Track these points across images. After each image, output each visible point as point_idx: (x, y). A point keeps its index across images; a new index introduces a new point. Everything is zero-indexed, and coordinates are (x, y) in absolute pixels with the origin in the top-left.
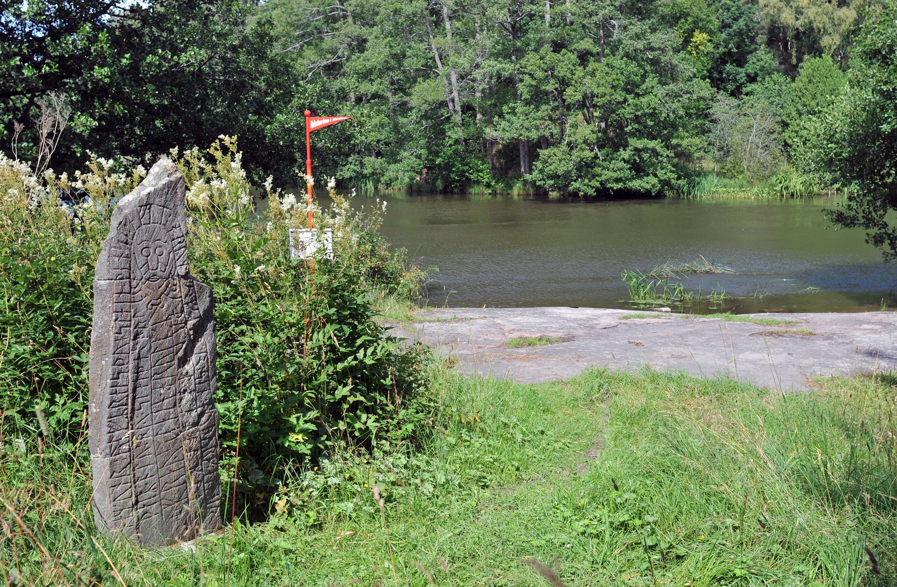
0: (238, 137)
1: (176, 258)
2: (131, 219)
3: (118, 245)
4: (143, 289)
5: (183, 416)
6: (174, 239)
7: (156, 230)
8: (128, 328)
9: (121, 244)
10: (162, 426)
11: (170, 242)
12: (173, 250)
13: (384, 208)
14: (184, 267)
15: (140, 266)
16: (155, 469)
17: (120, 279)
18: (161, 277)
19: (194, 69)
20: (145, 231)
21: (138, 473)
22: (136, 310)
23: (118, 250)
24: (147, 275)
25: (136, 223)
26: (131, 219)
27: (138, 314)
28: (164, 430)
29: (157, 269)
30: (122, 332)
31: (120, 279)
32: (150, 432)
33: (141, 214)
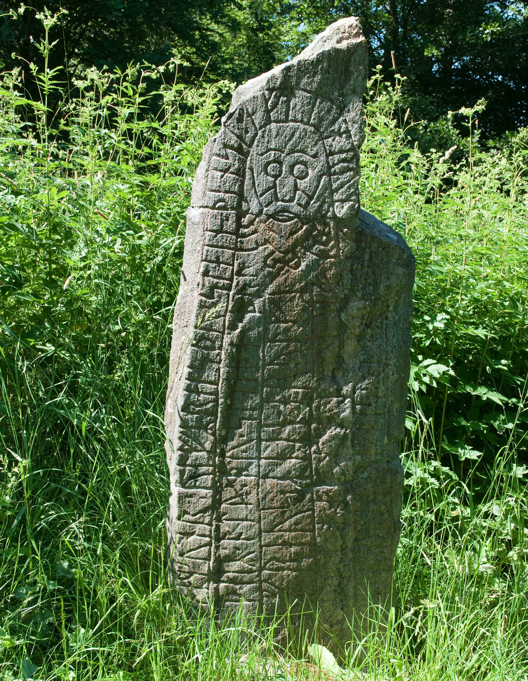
0: (482, 131)
1: (335, 186)
2: (250, 110)
3: (223, 152)
4: (260, 230)
5: (320, 460)
6: (332, 154)
7: (297, 135)
8: (225, 292)
9: (229, 151)
10: (277, 465)
11: (323, 158)
12: (328, 171)
13: (390, 477)
14: (347, 205)
15: (259, 190)
16: (255, 530)
17: (219, 208)
18: (297, 215)
19: (436, 263)
20: (274, 133)
21: (225, 526)
22: (244, 264)
23: (224, 160)
24: (271, 209)
25: (258, 118)
26: (250, 110)
27: (246, 271)
28: (279, 471)
29: (292, 200)
30: (216, 295)
31: (219, 208)
32: (253, 469)
33: (269, 103)
